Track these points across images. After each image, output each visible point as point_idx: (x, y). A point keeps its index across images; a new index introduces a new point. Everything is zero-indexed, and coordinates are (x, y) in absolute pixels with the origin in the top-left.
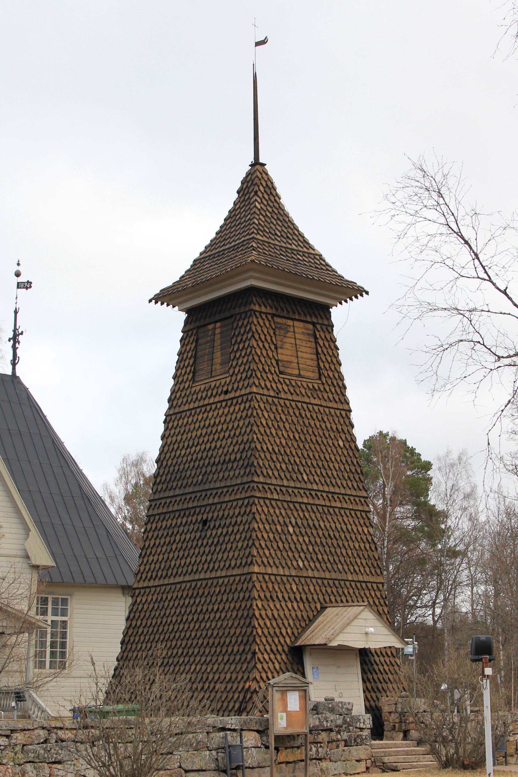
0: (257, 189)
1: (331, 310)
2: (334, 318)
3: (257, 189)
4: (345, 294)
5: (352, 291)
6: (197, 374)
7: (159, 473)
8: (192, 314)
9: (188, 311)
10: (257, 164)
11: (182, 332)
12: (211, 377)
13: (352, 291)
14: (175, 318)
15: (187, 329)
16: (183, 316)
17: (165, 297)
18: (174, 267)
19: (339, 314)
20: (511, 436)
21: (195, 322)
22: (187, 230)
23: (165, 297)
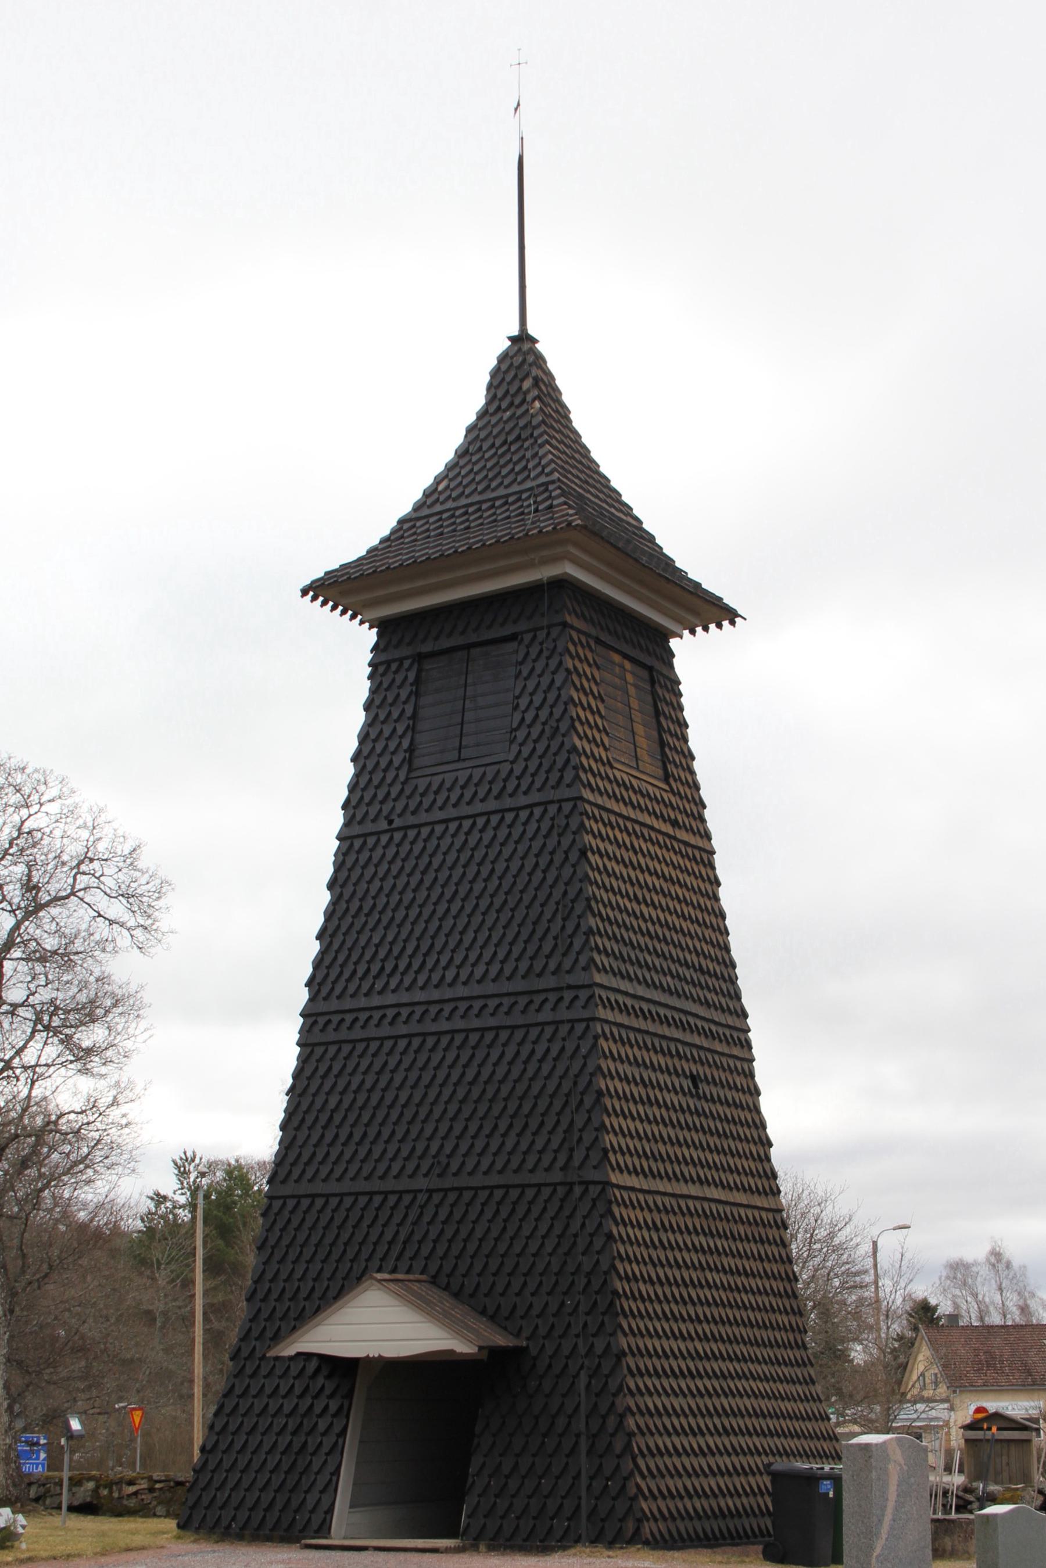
0: (522, 383)
1: (674, 643)
2: (680, 666)
3: (522, 383)
4: (696, 613)
5: (710, 611)
6: (416, 753)
7: (436, 489)
8: (392, 634)
9: (386, 628)
10: (523, 341)
11: (338, 838)
12: (459, 760)
13: (710, 611)
14: (353, 642)
15: (376, 661)
16: (370, 636)
17: (336, 589)
18: (364, 516)
19: (693, 655)
20: (150, 921)
21: (396, 647)
22: (391, 455)
23: (336, 589)
